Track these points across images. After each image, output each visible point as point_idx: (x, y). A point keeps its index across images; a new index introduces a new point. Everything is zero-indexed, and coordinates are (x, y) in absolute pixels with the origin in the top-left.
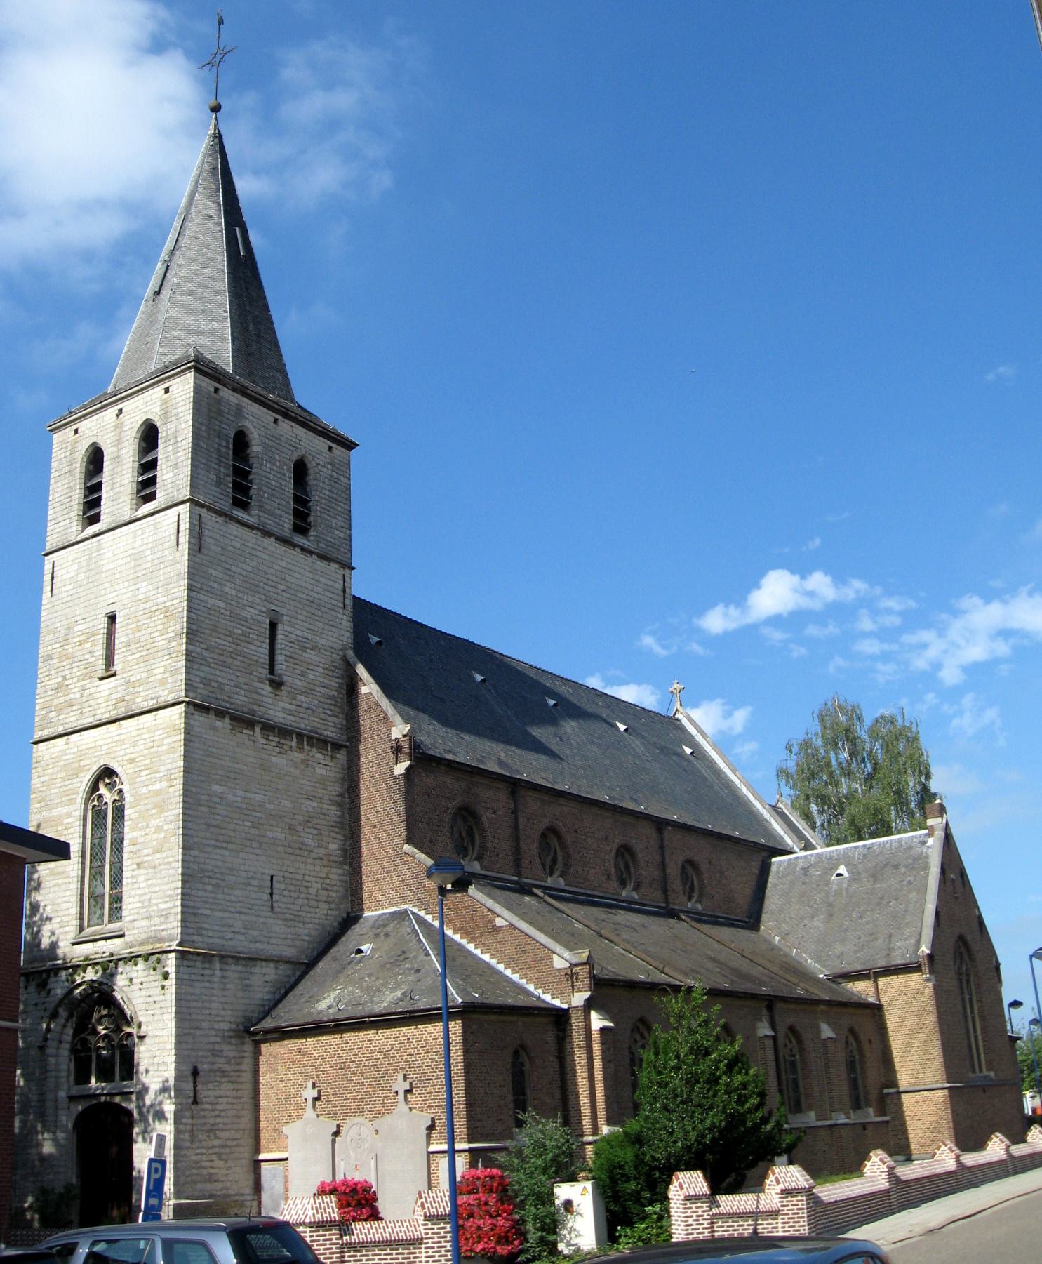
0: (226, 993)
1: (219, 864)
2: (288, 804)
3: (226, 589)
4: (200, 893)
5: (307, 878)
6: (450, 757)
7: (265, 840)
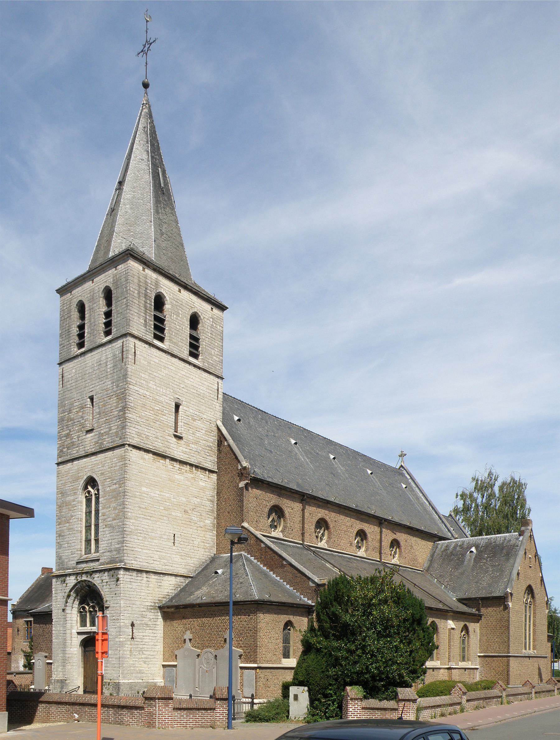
0: (148, 589)
1: (146, 527)
2: (184, 499)
3: (150, 385)
4: (136, 541)
5: (193, 536)
6: (270, 480)
7: (171, 516)
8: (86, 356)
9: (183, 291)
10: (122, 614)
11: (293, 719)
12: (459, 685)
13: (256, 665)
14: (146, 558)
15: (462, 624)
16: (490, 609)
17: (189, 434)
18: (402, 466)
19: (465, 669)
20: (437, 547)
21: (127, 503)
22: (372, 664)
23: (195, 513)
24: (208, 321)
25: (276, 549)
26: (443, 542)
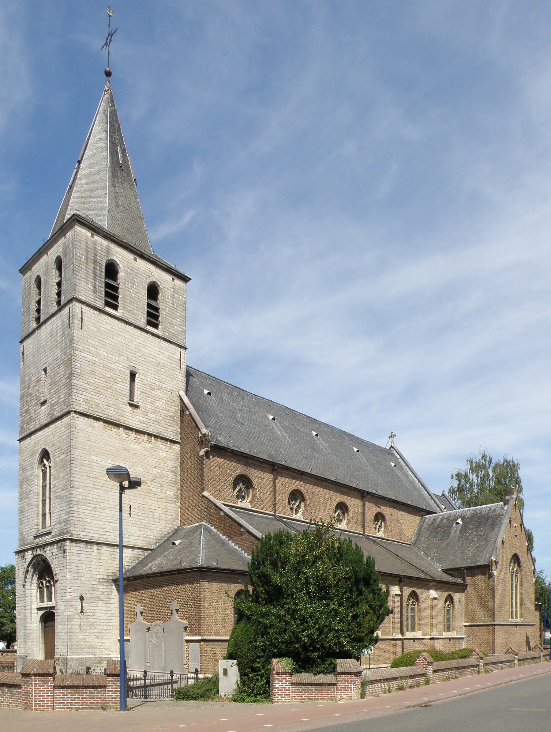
1: (96, 497)
3: (100, 352)
5: (153, 507)
8: (41, 329)
9: (139, 260)
10: (68, 587)
11: (223, 696)
12: (423, 654)
13: (199, 638)
14: (96, 529)
15: (446, 594)
16: (475, 578)
17: (147, 403)
18: (392, 447)
19: (450, 639)
20: (424, 521)
21: (73, 472)
22: (303, 631)
23: (155, 484)
24: (169, 291)
25: (231, 513)
26: (430, 515)
